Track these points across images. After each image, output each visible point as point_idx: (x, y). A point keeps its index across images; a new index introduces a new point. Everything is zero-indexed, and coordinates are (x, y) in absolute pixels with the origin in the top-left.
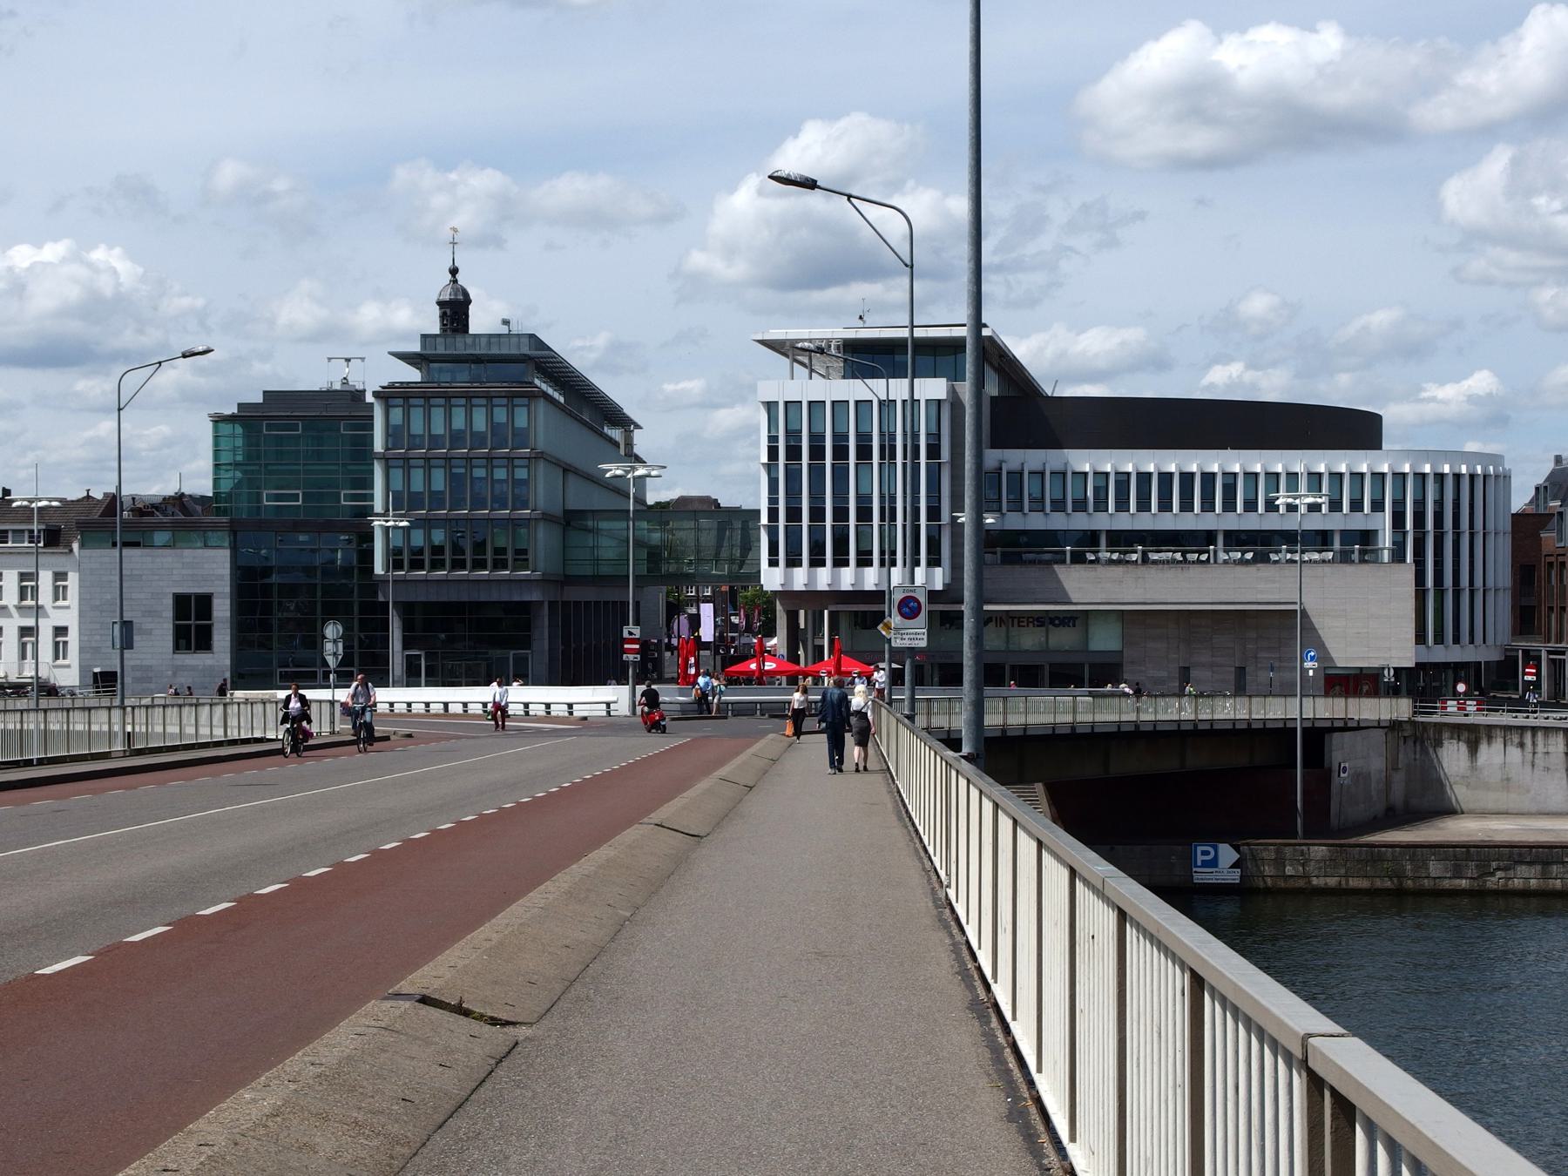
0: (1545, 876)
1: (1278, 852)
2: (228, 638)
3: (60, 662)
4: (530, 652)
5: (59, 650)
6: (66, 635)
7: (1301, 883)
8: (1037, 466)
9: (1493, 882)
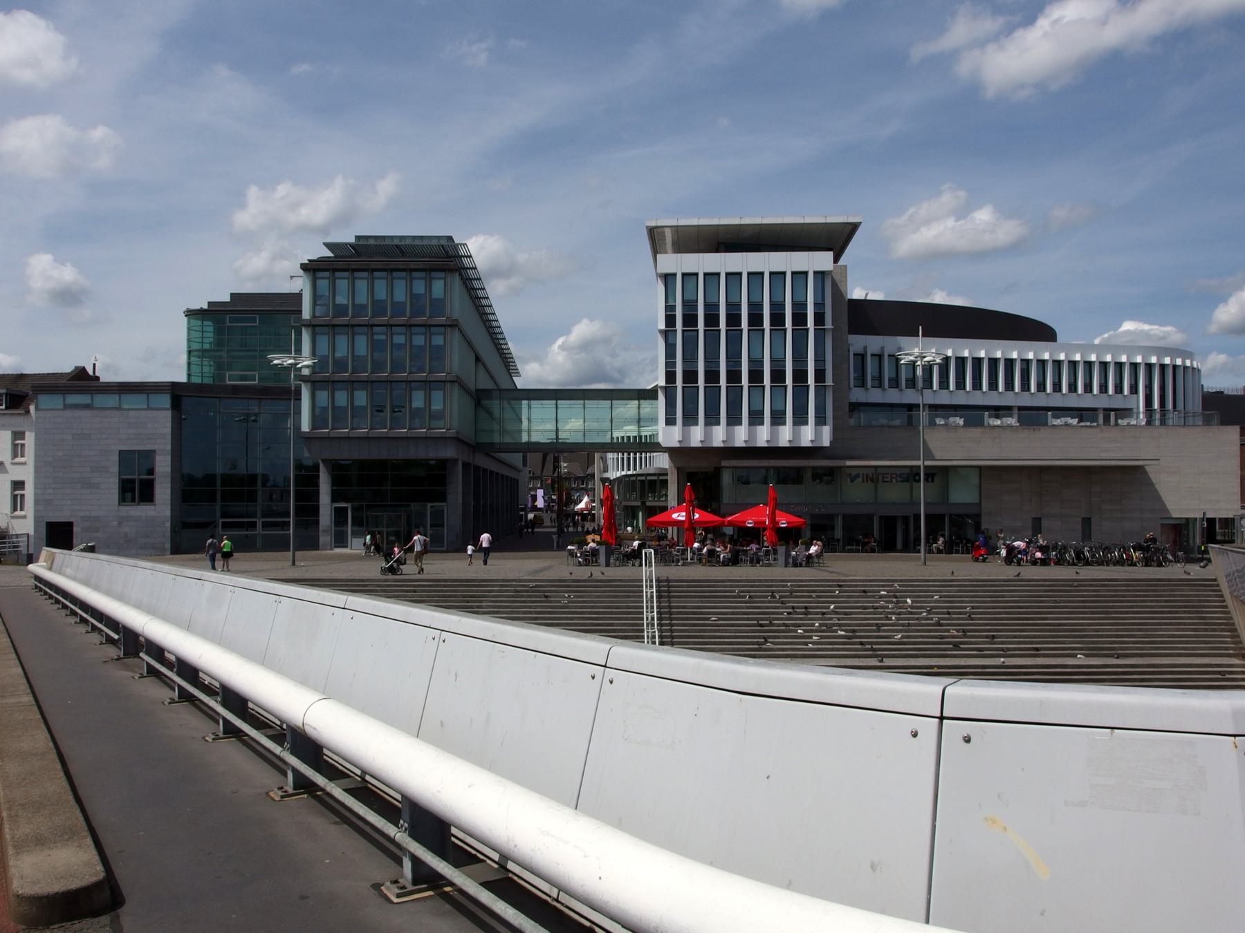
2: (169, 491)
3: (18, 513)
4: (444, 504)
6: (23, 489)
8: (877, 350)
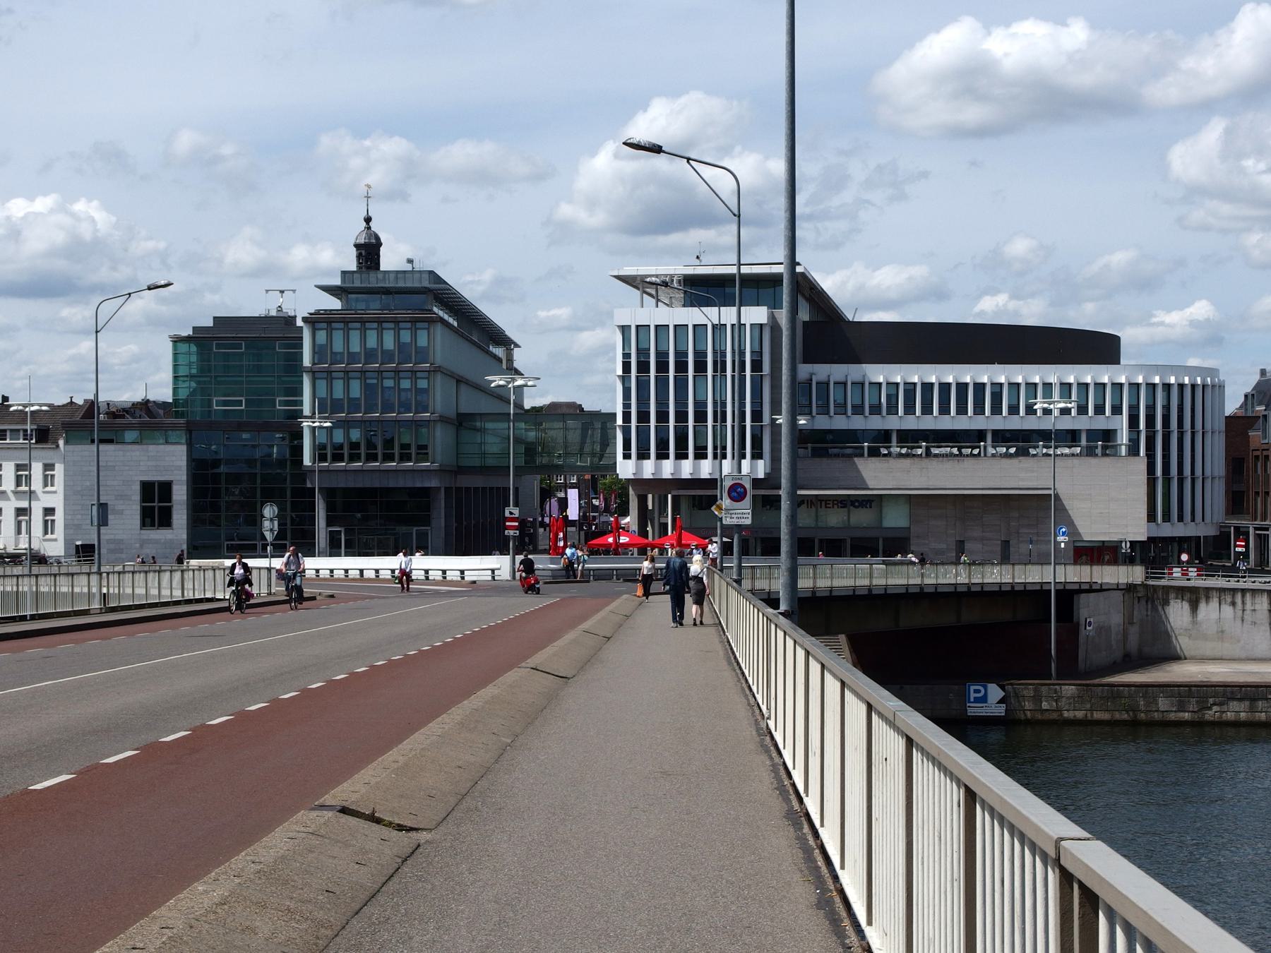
0: (1252, 710)
1: (1036, 690)
2: (185, 517)
3: (49, 536)
4: (429, 528)
5: (48, 527)
6: (54, 515)
7: (1055, 716)
8: (840, 378)
9: (1210, 715)
